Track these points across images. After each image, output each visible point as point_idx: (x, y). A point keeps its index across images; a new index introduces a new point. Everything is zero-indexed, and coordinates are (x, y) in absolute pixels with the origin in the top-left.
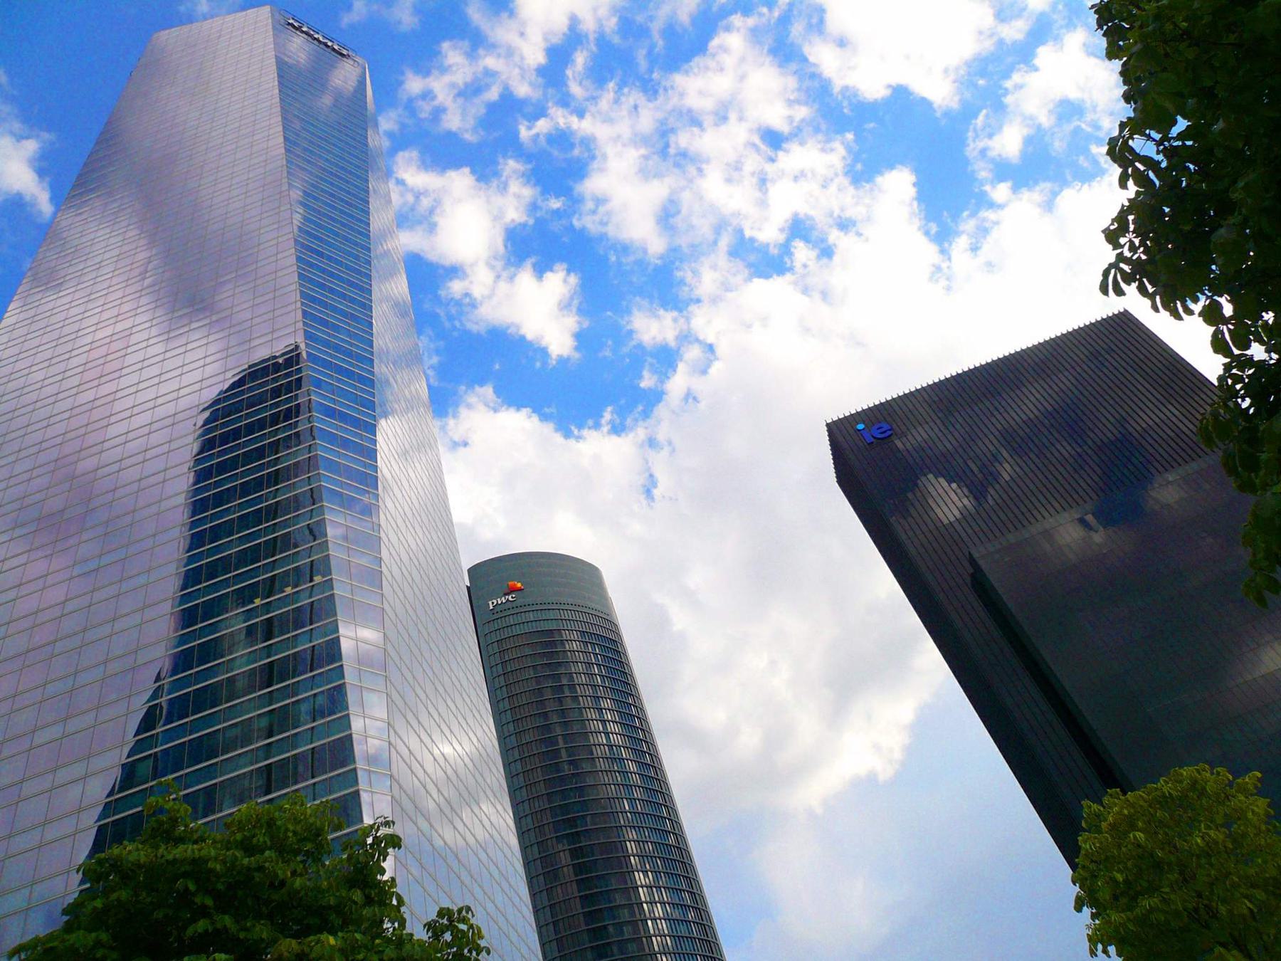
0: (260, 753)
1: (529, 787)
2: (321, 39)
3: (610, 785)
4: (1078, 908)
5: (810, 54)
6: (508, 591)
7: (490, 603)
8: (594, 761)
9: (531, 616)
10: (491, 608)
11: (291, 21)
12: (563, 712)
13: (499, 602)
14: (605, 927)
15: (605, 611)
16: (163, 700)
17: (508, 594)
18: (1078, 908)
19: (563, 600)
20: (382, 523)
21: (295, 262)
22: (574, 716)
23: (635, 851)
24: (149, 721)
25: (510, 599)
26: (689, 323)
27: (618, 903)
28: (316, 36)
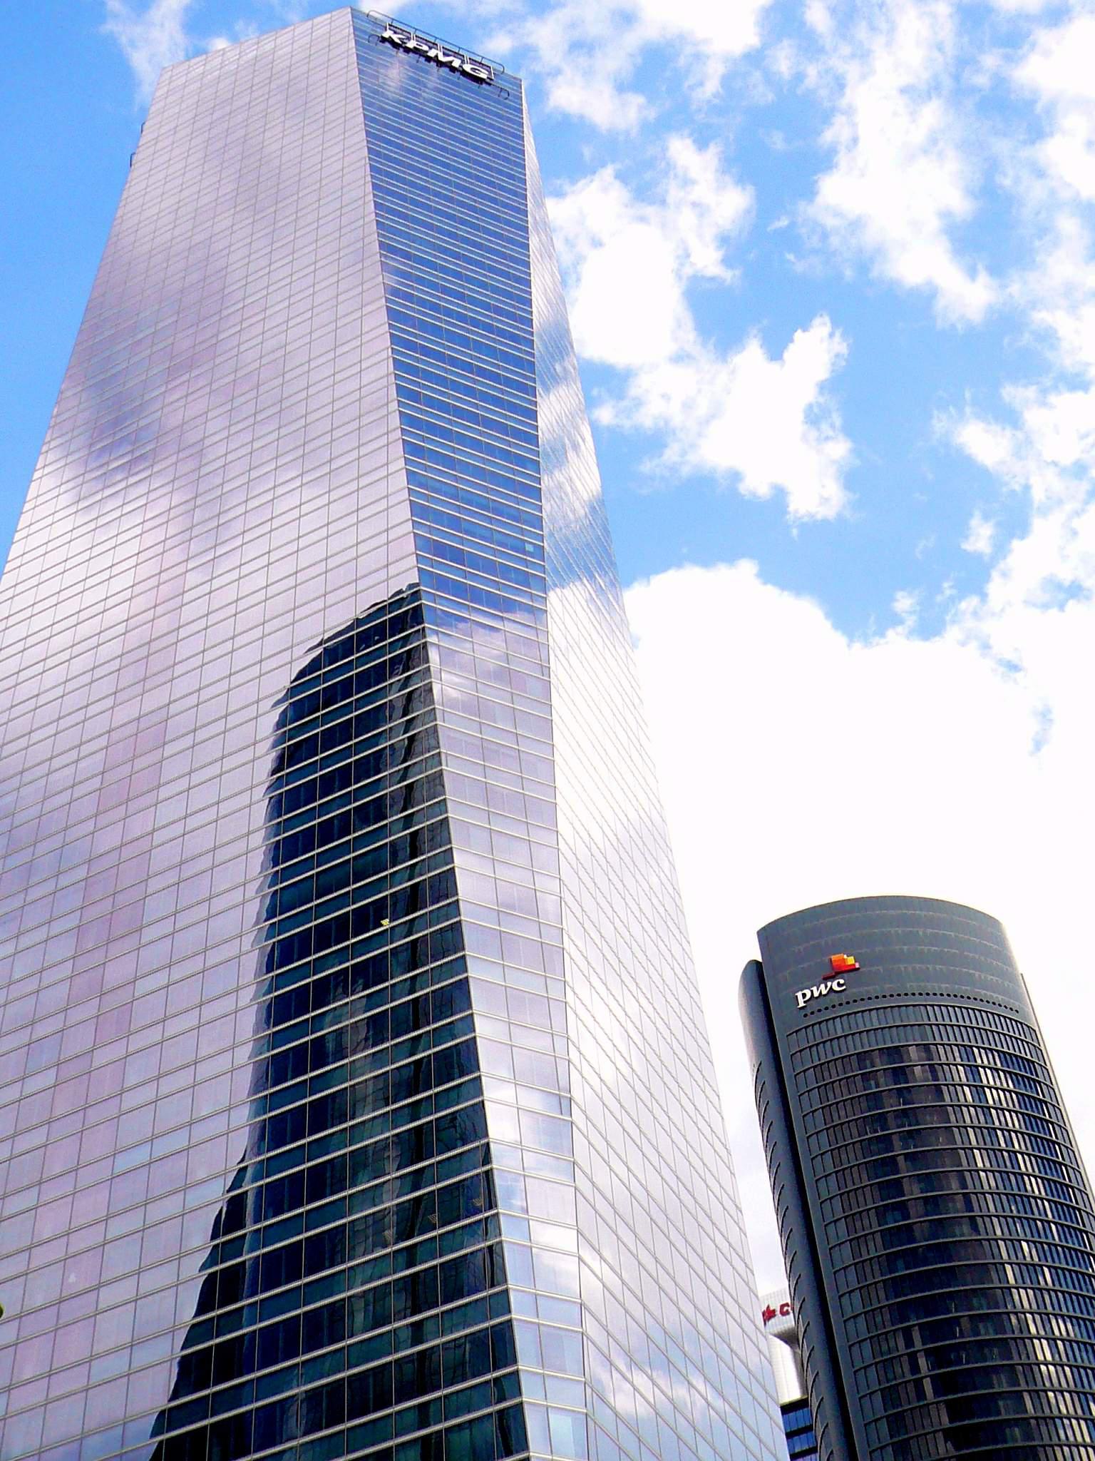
0: (401, 1259)
1: (854, 1243)
2: (441, 58)
3: (961, 1085)
4: (1052, 407)
5: (132, 43)
6: (829, 972)
7: (799, 995)
8: (988, 1271)
9: (874, 1021)
10: (802, 1004)
11: (387, 34)
12: (933, 1204)
13: (816, 994)
14: (956, 1321)
15: (1016, 1005)
16: (249, 1187)
17: (832, 978)
18: (1052, 407)
19: (930, 987)
20: (578, 1158)
21: (413, 550)
22: (956, 1210)
23: (1034, 1306)
24: (233, 1215)
25: (836, 988)
26: (765, 46)
27: (1004, 1416)
28: (432, 53)
